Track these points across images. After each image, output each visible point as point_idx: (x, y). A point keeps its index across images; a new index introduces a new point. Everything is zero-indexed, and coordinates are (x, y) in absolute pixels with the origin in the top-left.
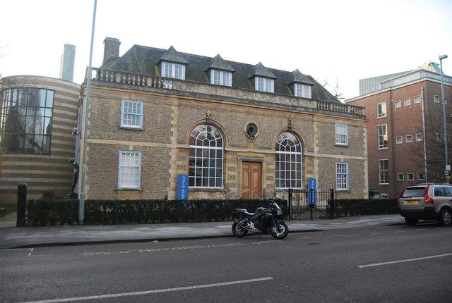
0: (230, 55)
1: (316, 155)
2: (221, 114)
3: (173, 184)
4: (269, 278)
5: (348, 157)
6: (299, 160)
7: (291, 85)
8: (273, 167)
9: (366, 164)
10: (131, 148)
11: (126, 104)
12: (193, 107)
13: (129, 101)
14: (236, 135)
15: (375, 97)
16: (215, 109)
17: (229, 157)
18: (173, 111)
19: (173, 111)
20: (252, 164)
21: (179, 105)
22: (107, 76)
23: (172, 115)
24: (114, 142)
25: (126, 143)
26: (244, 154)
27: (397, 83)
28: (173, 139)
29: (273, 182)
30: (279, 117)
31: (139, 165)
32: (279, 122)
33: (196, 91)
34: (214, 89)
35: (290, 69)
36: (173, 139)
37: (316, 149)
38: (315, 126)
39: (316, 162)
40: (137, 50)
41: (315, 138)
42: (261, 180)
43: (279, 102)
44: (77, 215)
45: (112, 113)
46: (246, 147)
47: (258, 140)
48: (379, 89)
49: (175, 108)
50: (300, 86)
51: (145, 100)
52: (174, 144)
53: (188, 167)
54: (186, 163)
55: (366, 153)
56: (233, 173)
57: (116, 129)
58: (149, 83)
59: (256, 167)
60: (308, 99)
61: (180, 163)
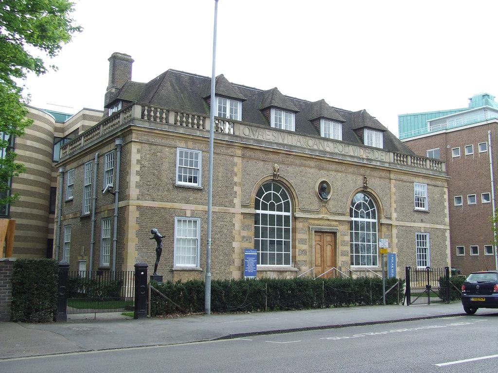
0: (291, 89)
1: (394, 223)
2: (290, 169)
3: (237, 263)
4: (440, 365)
5: (428, 225)
6: (287, 224)
7: (265, 111)
8: (348, 238)
9: (448, 234)
10: (188, 214)
11: (181, 153)
12: (258, 159)
13: (185, 150)
14: (306, 197)
15: (424, 141)
16: (283, 163)
17: (299, 225)
18: (235, 165)
19: (235, 165)
20: (325, 235)
21: (243, 157)
22: (196, 121)
23: (236, 169)
24: (169, 205)
25: (183, 206)
26: (316, 222)
27: (453, 125)
28: (237, 201)
29: (347, 259)
30: (353, 173)
31: (198, 237)
32: (354, 181)
33: (260, 138)
34: (276, 134)
35: (265, 86)
36: (237, 201)
37: (394, 215)
38: (392, 186)
39: (395, 231)
40: (171, 78)
41: (393, 200)
42: (335, 255)
43: (352, 154)
44: (202, 300)
45: (166, 166)
46: (318, 212)
47: (331, 203)
48: (428, 131)
49: (238, 160)
50: (328, 122)
51: (204, 149)
52: (238, 210)
53: (253, 239)
54: (251, 233)
55: (447, 220)
56: (304, 247)
57: (171, 188)
58: (172, 120)
59: (328, 238)
60: (290, 133)
61: (244, 233)
